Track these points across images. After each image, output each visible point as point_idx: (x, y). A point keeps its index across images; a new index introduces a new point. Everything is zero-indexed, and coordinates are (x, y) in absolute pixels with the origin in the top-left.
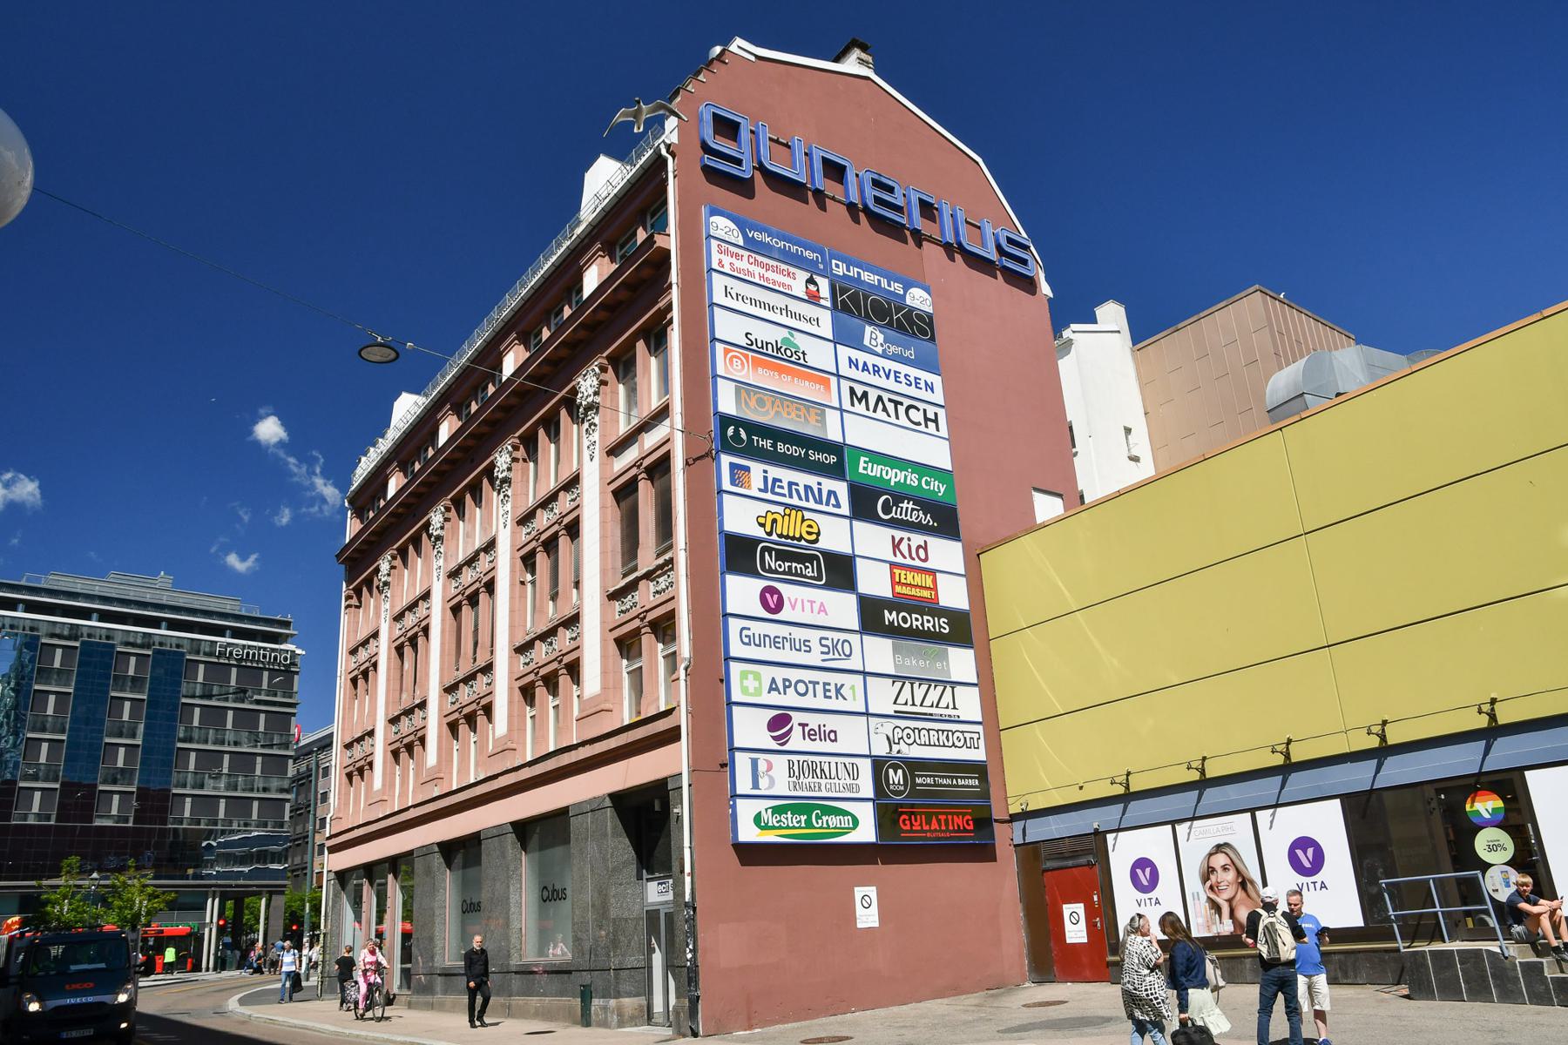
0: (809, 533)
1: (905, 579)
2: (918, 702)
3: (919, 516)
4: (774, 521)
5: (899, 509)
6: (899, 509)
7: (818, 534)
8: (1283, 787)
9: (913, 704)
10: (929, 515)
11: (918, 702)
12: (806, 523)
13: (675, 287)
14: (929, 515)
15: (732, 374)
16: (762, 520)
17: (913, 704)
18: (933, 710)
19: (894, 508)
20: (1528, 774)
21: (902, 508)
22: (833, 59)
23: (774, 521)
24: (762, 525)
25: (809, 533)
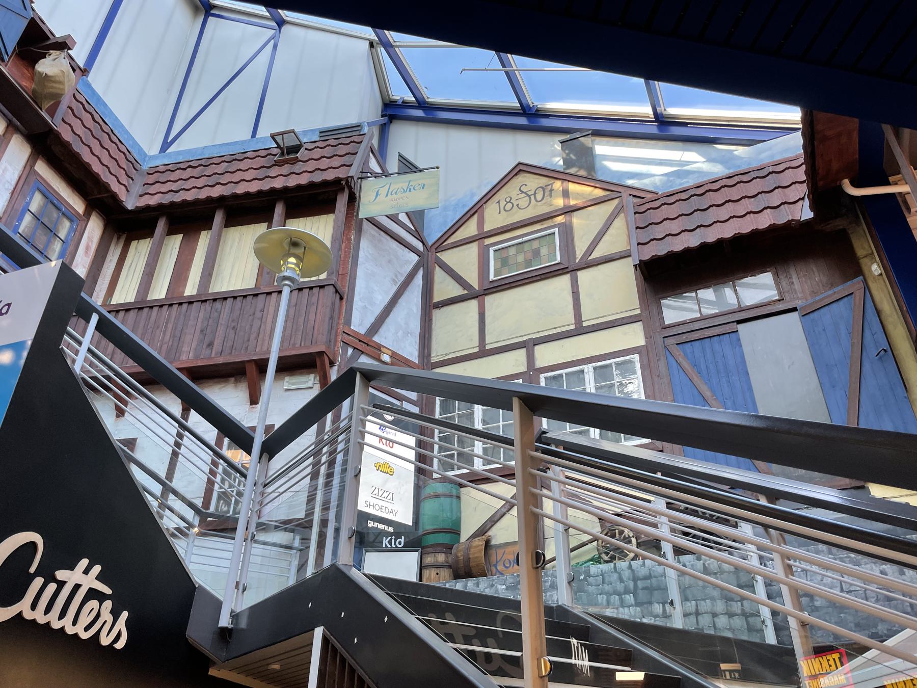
0: (391, 472)
1: (828, 660)
2: (380, 495)
3: (98, 616)
4: (380, 466)
5: (52, 587)
6: (52, 587)
7: (394, 473)
8: (524, 197)
9: (378, 496)
10: (125, 615)
11: (380, 495)
12: (390, 468)
13: (785, 578)
14: (125, 615)
15: (306, 285)
16: (376, 465)
17: (378, 496)
18: (385, 499)
19: (39, 581)
20: (367, 422)
21: (61, 584)
22: (310, 531)
23: (380, 466)
24: (376, 467)
25: (391, 472)
